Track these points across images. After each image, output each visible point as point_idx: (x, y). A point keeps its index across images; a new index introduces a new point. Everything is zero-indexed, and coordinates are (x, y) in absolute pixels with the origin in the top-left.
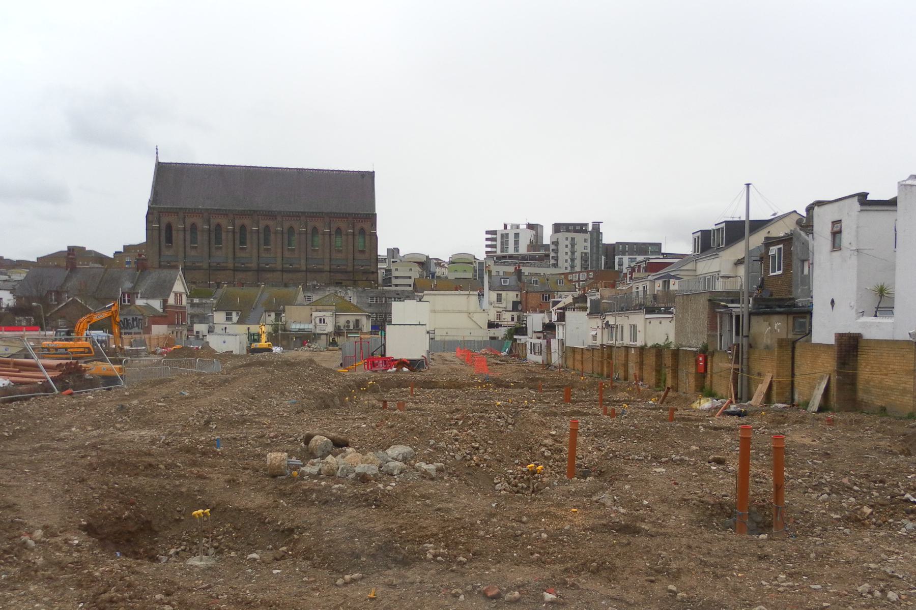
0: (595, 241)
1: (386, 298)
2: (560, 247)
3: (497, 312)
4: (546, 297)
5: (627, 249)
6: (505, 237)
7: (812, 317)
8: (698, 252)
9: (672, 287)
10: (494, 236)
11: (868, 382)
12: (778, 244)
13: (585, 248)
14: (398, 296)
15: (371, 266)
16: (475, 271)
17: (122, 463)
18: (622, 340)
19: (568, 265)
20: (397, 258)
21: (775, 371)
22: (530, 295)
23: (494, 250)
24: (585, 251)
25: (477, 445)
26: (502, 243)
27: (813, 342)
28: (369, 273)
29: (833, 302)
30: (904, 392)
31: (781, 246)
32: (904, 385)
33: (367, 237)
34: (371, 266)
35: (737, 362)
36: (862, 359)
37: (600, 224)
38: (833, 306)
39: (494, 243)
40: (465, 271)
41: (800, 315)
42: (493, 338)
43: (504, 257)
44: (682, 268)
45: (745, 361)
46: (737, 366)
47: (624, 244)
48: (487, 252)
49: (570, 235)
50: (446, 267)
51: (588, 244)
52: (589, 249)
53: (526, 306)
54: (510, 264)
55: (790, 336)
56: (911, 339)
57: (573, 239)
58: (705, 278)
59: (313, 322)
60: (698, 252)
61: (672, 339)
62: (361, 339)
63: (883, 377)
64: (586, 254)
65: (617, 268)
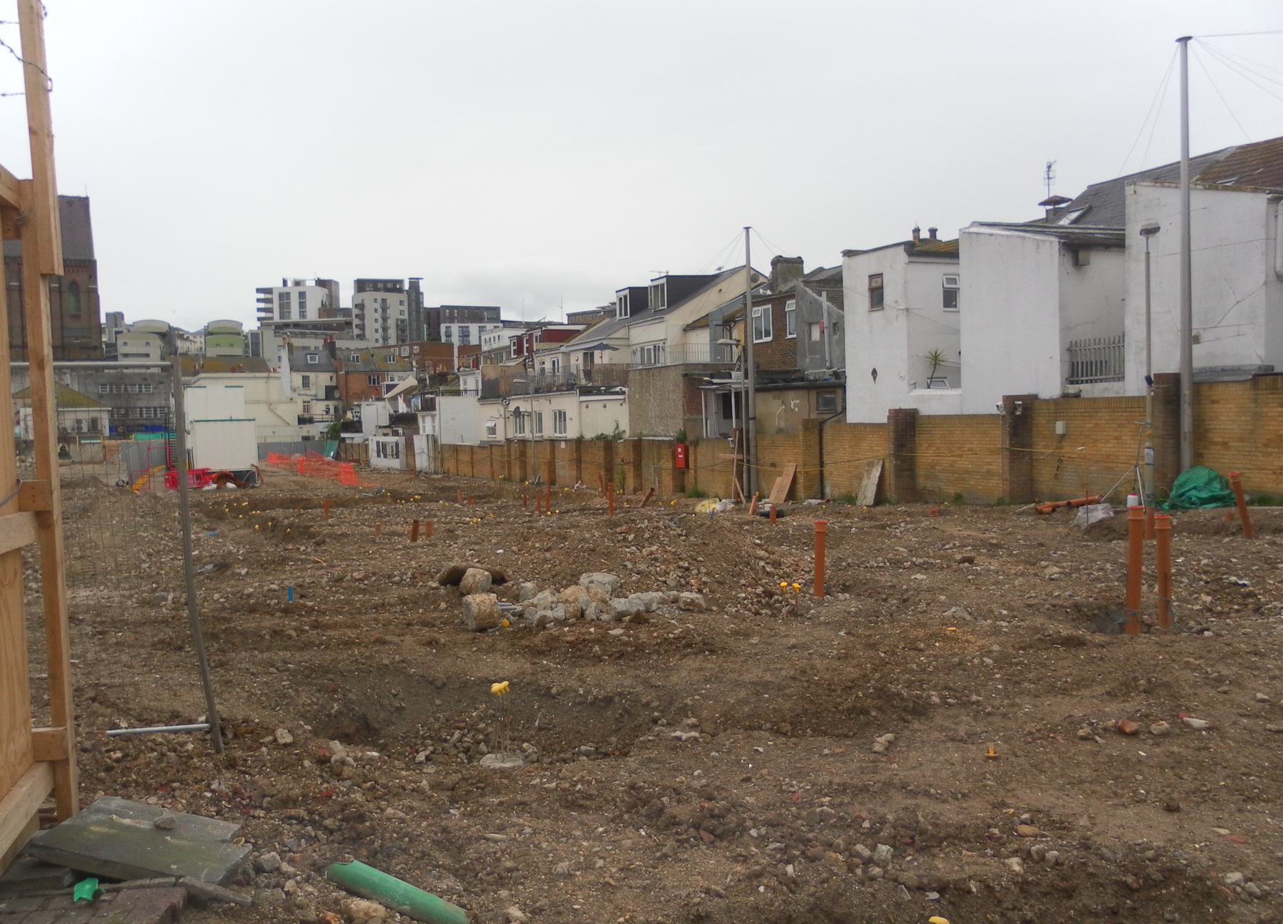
0: (414, 304)
1: (125, 385)
2: (366, 312)
3: (304, 402)
4: (374, 380)
5: (456, 315)
6: (284, 297)
7: (845, 391)
8: (626, 314)
9: (597, 360)
10: (268, 296)
11: (932, 466)
12: (765, 304)
13: (401, 313)
14: (145, 382)
15: (90, 338)
16: (247, 346)
17: (233, 634)
18: (541, 431)
19: (379, 335)
20: (121, 327)
21: (800, 459)
22: (351, 377)
23: (269, 315)
24: (402, 317)
25: (687, 565)
26: (281, 306)
27: (848, 422)
28: (90, 348)
29: (874, 373)
30: (989, 474)
31: (769, 306)
32: (988, 467)
33: (83, 297)
34: (90, 338)
35: (740, 451)
36: (922, 440)
37: (420, 281)
38: (875, 378)
39: (268, 306)
40: (232, 345)
41: (830, 390)
42: (306, 438)
43: (287, 325)
44: (612, 336)
45: (752, 449)
46: (740, 457)
47: (451, 308)
48: (259, 319)
49: (380, 295)
50: (191, 341)
51: (405, 308)
52: (406, 313)
53: (347, 393)
54: (316, 336)
55: (813, 416)
56: (999, 413)
57: (384, 301)
58: (642, 349)
59: (22, 423)
60: (626, 314)
61: (625, 426)
62: (104, 447)
63: (955, 459)
64: (403, 321)
65: (444, 339)
